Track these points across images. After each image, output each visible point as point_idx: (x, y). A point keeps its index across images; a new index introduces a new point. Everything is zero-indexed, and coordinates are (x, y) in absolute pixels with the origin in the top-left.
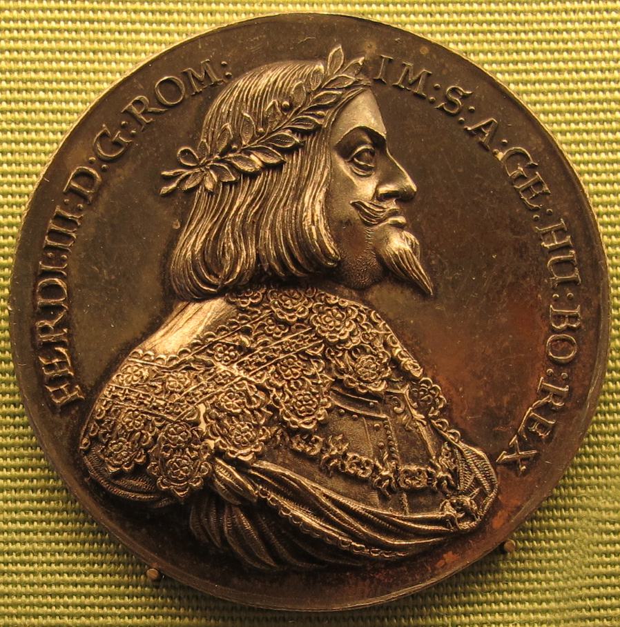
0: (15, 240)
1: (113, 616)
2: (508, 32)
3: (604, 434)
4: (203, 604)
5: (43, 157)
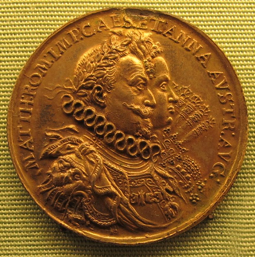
3: (247, 173)
4: (84, 243)
5: (7, 98)
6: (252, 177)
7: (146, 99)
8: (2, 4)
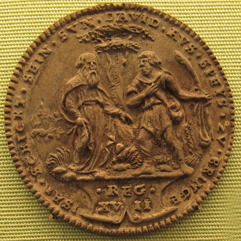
0: (5, 135)
1: (18, 237)
2: (219, 17)
7: (130, 46)
8: (0, 3)
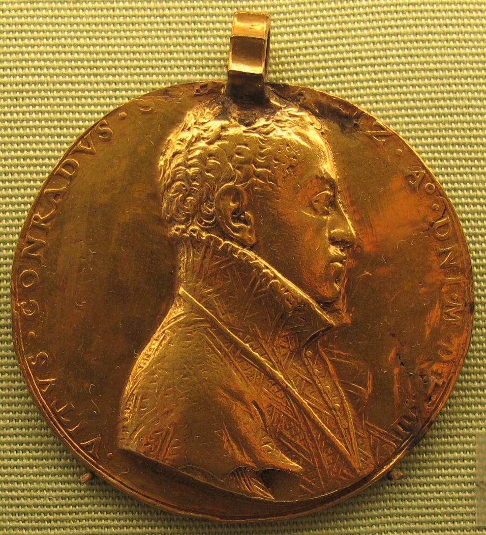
4: (162, 516)
6: (481, 358)
